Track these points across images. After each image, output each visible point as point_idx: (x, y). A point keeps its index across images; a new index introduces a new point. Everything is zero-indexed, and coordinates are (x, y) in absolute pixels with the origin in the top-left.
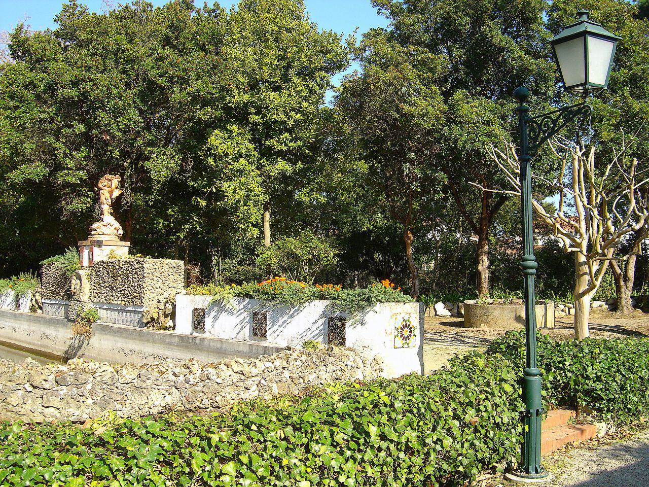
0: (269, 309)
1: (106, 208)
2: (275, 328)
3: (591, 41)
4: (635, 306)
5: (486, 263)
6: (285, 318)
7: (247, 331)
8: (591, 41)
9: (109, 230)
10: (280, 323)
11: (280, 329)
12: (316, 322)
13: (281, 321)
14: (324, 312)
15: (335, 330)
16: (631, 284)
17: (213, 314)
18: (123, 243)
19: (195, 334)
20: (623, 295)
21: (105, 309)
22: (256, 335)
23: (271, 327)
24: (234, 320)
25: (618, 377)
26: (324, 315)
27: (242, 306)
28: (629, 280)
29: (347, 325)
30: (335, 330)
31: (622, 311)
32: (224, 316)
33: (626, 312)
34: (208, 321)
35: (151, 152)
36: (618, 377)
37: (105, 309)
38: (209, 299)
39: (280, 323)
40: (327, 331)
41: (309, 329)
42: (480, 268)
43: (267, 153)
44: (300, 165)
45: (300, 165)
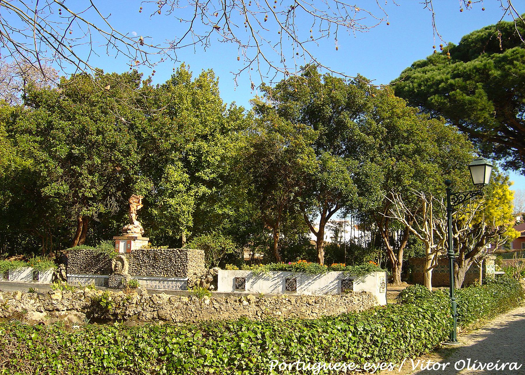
0: (298, 276)
1: (134, 216)
2: (302, 286)
3: (487, 167)
4: (402, 281)
5: (323, 254)
6: (310, 281)
7: (280, 288)
8: (487, 167)
9: (138, 230)
10: (306, 283)
11: (306, 287)
12: (332, 282)
13: (306, 283)
14: (338, 277)
15: (345, 286)
16: (401, 267)
17: (251, 281)
18: (145, 238)
19: (235, 292)
20: (397, 273)
21: (145, 280)
22: (288, 290)
23: (300, 286)
24: (270, 283)
25: (466, 306)
26: (338, 278)
27: (276, 275)
28: (400, 264)
29: (354, 283)
30: (345, 286)
31: (397, 283)
32: (260, 282)
33: (399, 284)
34: (247, 285)
35: (137, 179)
36: (466, 306)
37: (145, 280)
38: (249, 272)
39: (306, 283)
40: (340, 286)
41: (327, 286)
42: (319, 256)
43: (195, 180)
44: (214, 189)
45: (214, 189)
